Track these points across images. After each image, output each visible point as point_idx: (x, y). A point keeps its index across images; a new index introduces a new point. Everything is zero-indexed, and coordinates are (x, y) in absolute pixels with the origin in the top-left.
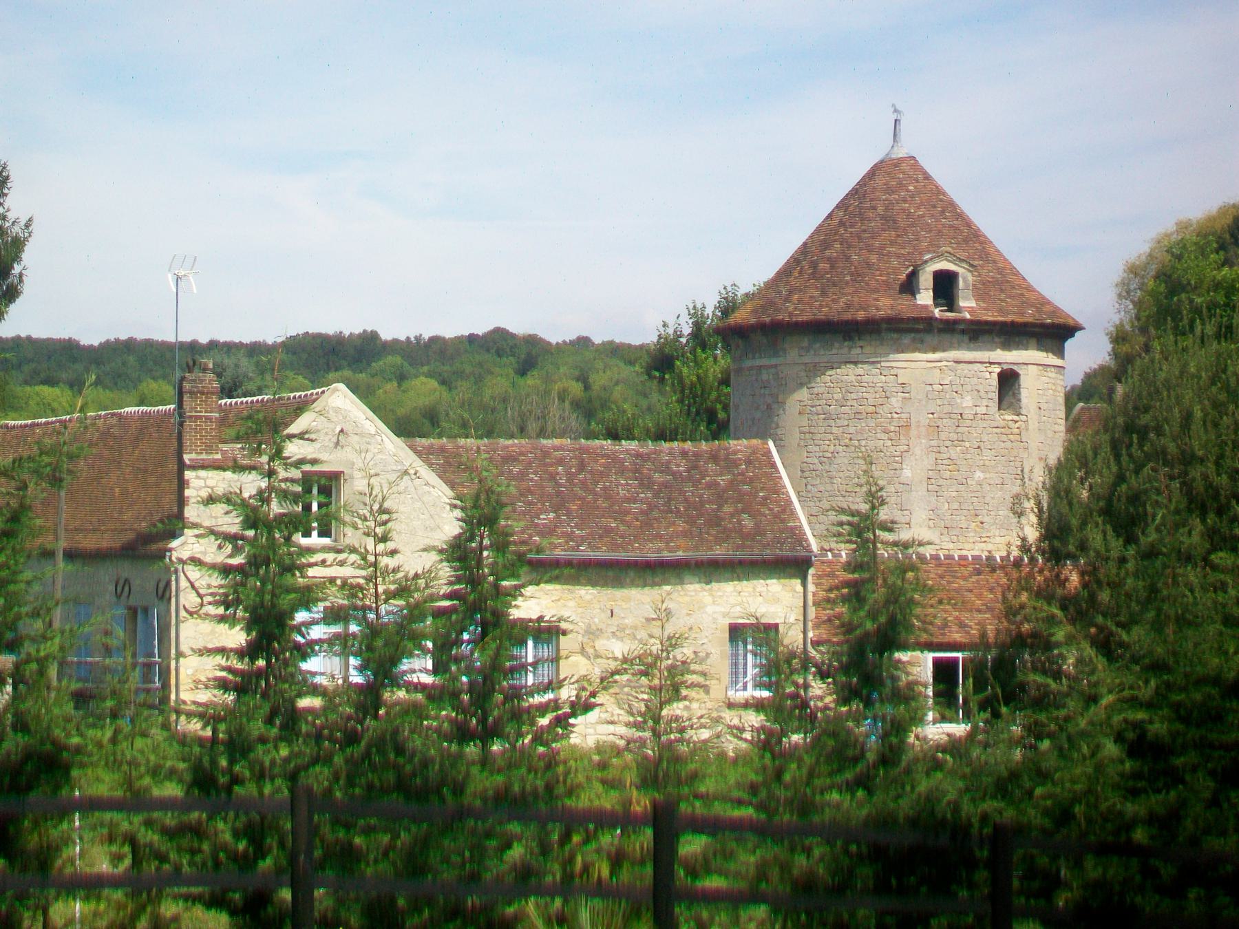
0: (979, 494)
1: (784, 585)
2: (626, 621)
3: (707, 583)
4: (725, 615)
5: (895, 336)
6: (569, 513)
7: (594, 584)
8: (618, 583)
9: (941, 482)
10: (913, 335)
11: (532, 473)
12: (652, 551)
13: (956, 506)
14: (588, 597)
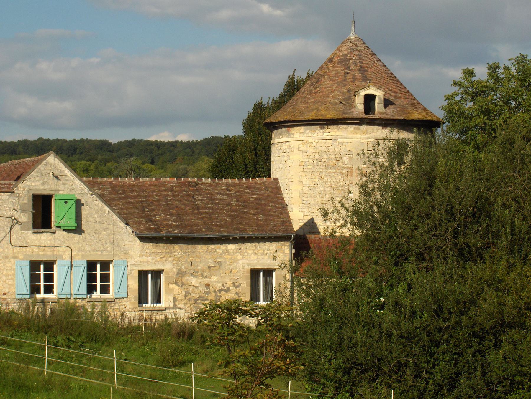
4: (248, 264)
5: (345, 126)
6: (171, 215)
10: (354, 126)
11: (155, 195)
12: (210, 234)
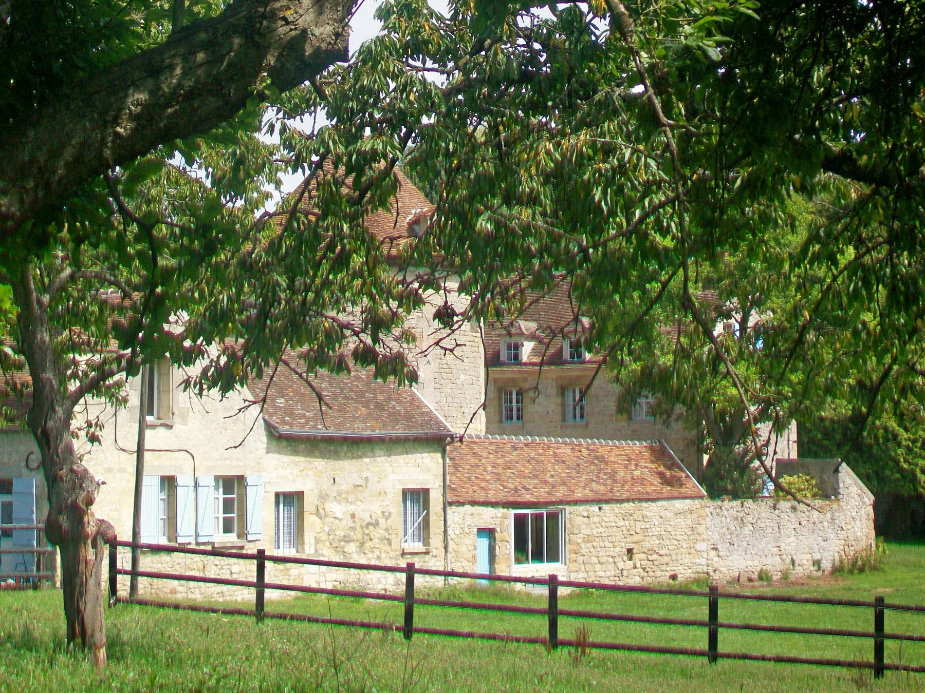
0: (462, 391)
1: (432, 458)
2: (342, 487)
3: (389, 456)
7: (323, 456)
8: (336, 456)
9: (442, 382)
13: (450, 400)
14: (320, 468)
